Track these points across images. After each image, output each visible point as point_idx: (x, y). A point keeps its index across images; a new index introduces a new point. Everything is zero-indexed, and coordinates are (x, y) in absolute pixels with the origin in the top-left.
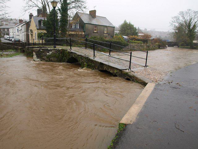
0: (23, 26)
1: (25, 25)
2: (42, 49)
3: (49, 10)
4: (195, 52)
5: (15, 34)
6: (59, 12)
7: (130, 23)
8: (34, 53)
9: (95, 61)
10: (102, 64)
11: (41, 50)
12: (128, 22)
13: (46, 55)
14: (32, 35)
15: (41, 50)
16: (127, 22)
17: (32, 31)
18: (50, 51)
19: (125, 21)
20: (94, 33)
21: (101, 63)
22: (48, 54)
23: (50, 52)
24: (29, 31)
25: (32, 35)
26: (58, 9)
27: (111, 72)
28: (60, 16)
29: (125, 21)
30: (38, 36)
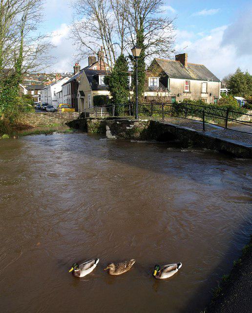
0: (65, 86)
1: (70, 84)
2: (119, 121)
3: (115, 59)
4: (242, 159)
5: (49, 99)
6: (129, 60)
7: (247, 73)
8: (108, 128)
9: (207, 137)
10: (218, 141)
11: (118, 123)
12: (243, 71)
13: (125, 130)
14: (83, 100)
15: (118, 123)
16: (242, 71)
17: (82, 93)
18: (131, 124)
19: (238, 70)
20: (184, 92)
21: (216, 139)
22: (128, 128)
23: (131, 126)
24: (79, 93)
25: (83, 100)
26: (128, 57)
27: (233, 152)
28: (132, 68)
29: (238, 70)
30: (94, 101)
